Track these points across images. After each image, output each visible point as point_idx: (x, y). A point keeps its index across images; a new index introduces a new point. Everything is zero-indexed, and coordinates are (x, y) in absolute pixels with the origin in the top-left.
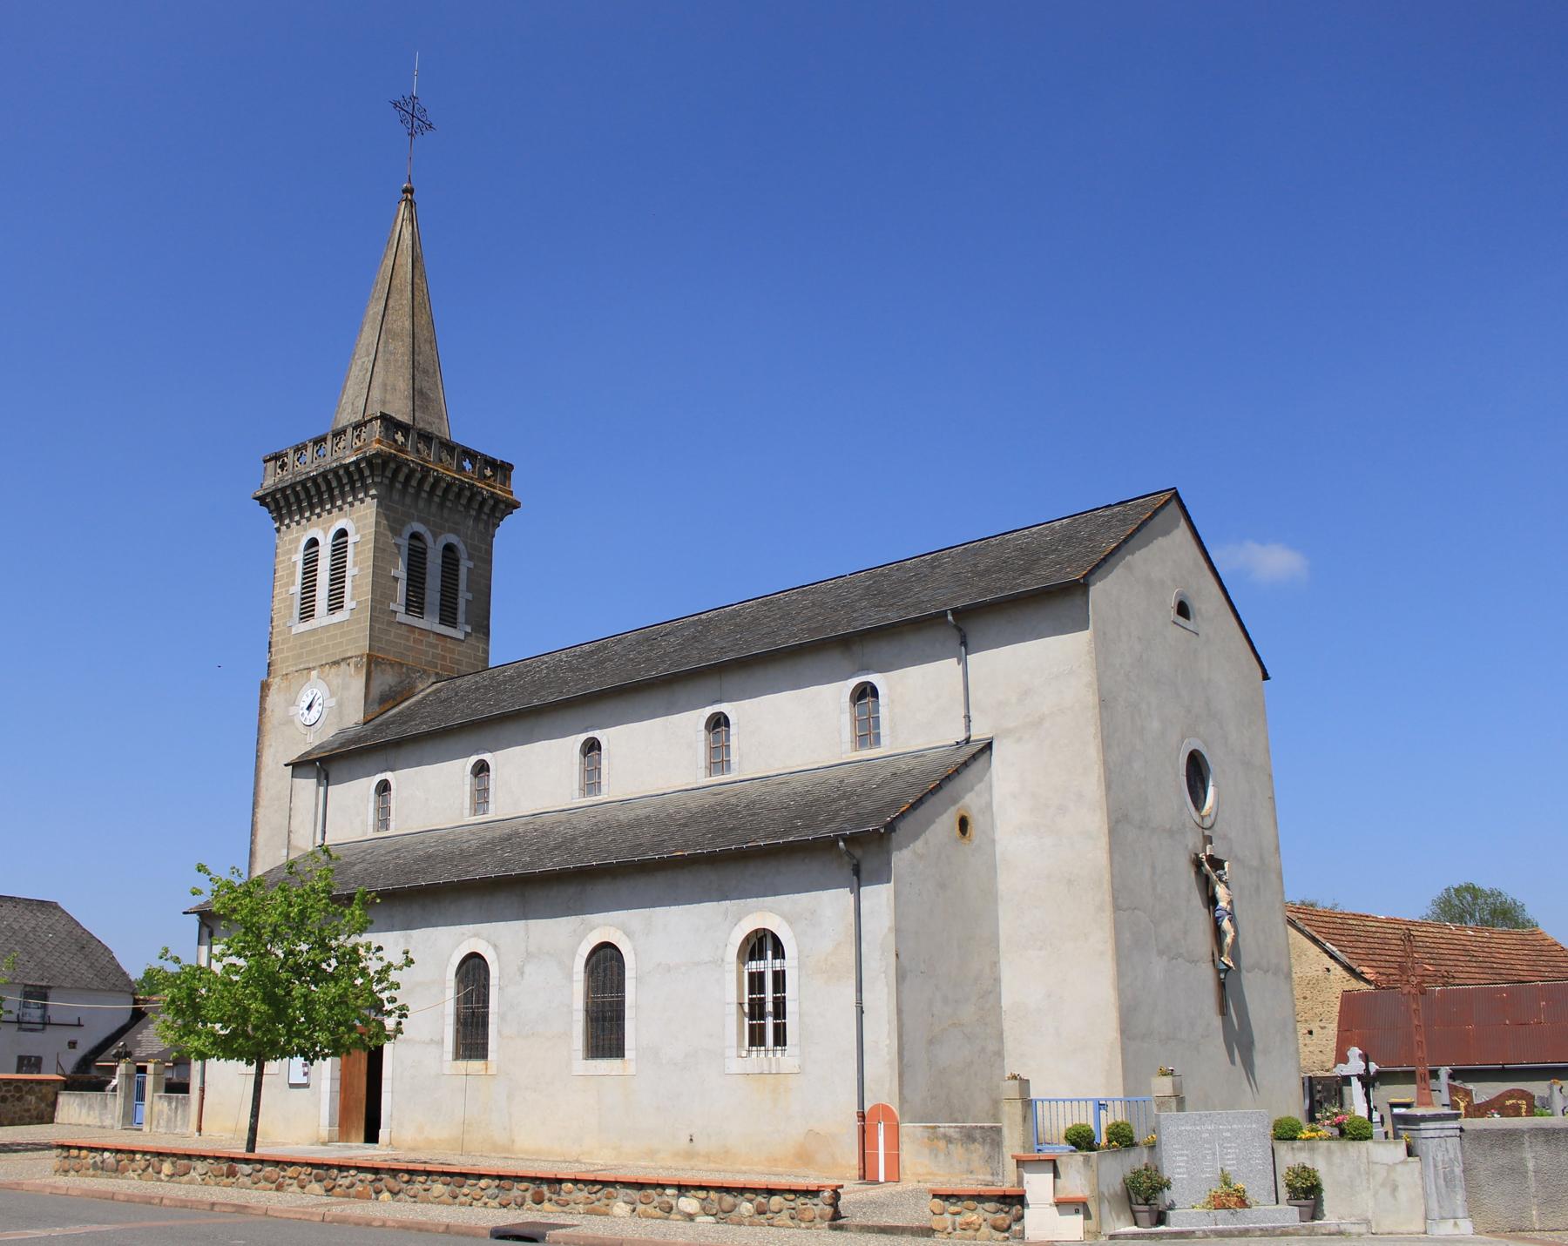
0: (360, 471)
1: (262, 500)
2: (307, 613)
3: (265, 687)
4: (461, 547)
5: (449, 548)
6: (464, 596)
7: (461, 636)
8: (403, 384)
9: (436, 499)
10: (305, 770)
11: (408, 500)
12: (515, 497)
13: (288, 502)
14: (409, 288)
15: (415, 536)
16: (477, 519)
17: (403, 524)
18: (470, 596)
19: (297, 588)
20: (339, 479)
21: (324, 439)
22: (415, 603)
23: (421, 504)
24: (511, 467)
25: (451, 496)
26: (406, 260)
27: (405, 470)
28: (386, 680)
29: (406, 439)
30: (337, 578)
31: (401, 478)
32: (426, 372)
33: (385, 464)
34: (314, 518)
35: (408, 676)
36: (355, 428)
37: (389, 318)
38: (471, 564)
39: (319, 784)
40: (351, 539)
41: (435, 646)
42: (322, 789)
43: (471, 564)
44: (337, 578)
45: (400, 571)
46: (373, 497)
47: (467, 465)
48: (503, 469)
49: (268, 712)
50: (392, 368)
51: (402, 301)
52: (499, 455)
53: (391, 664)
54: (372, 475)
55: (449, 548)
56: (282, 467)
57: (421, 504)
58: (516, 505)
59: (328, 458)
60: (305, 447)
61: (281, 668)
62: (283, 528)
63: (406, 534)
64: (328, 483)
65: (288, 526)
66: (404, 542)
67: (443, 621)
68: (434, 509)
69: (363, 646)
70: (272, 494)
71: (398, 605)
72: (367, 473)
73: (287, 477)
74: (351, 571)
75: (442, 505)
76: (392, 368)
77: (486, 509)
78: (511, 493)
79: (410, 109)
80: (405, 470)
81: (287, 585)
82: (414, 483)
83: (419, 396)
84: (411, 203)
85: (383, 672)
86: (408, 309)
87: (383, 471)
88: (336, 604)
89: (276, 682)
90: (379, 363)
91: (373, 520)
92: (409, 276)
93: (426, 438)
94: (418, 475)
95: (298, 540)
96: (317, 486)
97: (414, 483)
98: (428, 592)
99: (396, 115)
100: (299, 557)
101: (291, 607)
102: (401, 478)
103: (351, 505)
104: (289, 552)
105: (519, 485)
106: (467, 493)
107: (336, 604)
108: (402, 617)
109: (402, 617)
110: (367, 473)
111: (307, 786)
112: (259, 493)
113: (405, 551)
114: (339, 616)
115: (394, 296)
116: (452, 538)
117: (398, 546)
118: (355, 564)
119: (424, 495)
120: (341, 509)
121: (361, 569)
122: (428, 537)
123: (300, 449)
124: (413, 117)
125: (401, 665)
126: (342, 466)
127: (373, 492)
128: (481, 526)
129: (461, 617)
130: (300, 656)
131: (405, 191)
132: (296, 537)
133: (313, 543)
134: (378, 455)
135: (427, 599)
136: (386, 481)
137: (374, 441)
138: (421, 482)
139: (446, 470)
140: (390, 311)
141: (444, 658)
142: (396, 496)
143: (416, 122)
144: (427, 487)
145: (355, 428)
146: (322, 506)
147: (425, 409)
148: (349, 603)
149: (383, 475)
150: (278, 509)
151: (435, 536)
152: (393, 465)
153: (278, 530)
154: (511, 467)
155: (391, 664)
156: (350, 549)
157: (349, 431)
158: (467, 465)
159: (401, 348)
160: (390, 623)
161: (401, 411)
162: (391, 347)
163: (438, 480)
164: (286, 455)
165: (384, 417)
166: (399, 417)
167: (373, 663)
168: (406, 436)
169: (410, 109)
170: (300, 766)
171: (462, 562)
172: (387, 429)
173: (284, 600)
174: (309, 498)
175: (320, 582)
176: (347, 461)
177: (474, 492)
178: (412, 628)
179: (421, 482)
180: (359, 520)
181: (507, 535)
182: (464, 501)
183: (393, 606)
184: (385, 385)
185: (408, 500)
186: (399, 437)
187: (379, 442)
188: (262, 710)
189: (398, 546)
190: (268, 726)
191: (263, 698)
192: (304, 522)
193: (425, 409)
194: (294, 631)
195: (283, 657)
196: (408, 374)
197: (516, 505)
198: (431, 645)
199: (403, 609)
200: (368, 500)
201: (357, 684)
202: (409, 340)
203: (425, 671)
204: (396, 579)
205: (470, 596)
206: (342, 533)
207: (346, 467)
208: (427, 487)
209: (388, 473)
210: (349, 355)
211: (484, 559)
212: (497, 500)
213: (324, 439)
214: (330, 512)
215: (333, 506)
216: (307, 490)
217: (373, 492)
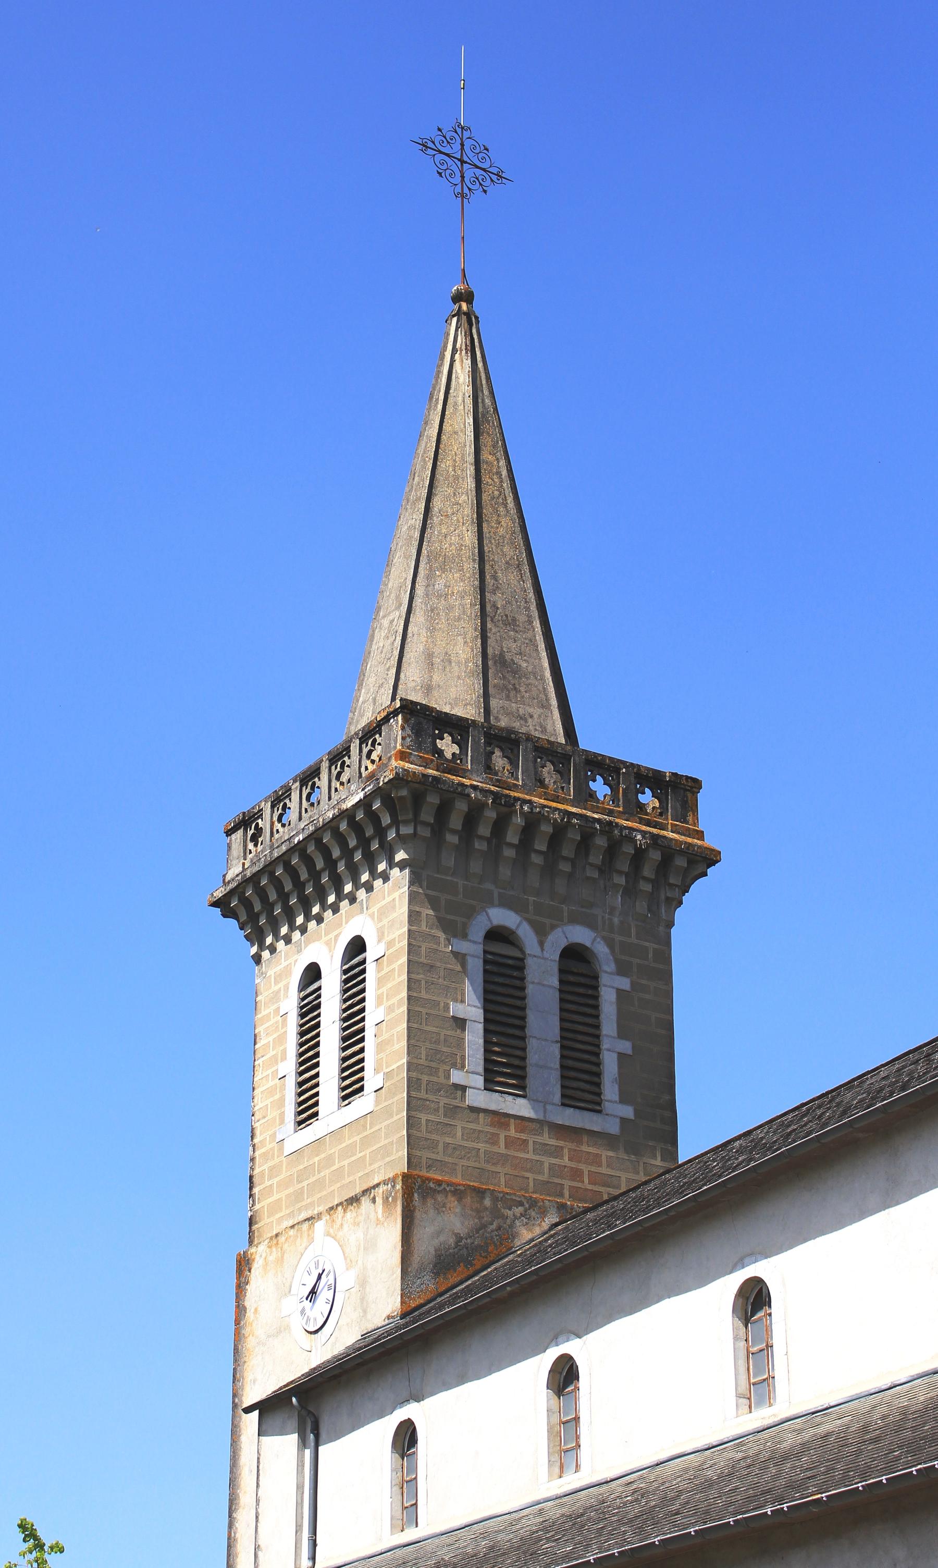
0: (373, 817)
1: (215, 904)
2: (307, 1111)
3: (243, 1264)
4: (601, 950)
5: (574, 956)
6: (612, 1049)
7: (613, 1128)
8: (463, 650)
9: (537, 859)
10: (276, 1419)
11: (476, 866)
12: (710, 841)
13: (267, 903)
14: (471, 470)
15: (496, 935)
16: (630, 892)
17: (470, 913)
18: (626, 1046)
19: (289, 1066)
20: (341, 839)
21: (314, 772)
22: (504, 1069)
23: (505, 872)
24: (696, 784)
25: (567, 851)
26: (462, 422)
27: (461, 806)
28: (447, 1224)
29: (462, 745)
30: (353, 1036)
31: (456, 821)
32: (510, 622)
33: (418, 799)
34: (312, 925)
35: (496, 1214)
36: (363, 740)
37: (433, 533)
38: (624, 983)
39: (303, 1443)
40: (371, 954)
41: (557, 1152)
42: (308, 1453)
43: (624, 983)
44: (353, 1036)
45: (470, 1007)
46: (402, 865)
47: (599, 787)
48: (680, 791)
49: (250, 1314)
50: (442, 624)
51: (456, 499)
52: (666, 763)
53: (459, 1193)
54: (396, 823)
55: (574, 956)
56: (254, 839)
57: (505, 872)
58: (711, 858)
59: (324, 805)
60: (287, 791)
61: (268, 1225)
62: (266, 954)
63: (478, 929)
64: (325, 851)
65: (273, 949)
66: (473, 948)
67: (569, 1099)
68: (534, 879)
69: (396, 1160)
70: (237, 891)
71: (469, 1074)
72: (386, 820)
73: (263, 852)
74: (373, 1014)
75: (549, 870)
76: (442, 624)
77: (648, 871)
78: (700, 835)
79: (455, 149)
80: (461, 806)
81: (275, 1060)
82: (484, 830)
83: (493, 667)
84: (470, 320)
85: (440, 1209)
86: (468, 511)
87: (416, 814)
88: (351, 1088)
89: (260, 1253)
90: (418, 617)
91: (405, 909)
92: (470, 449)
93: (508, 741)
94: (491, 814)
95: (287, 971)
96: (308, 861)
97: (484, 830)
98: (532, 1045)
99: (427, 164)
100: (291, 1003)
101: (281, 1102)
102: (456, 821)
103: (369, 888)
104: (275, 997)
105: (714, 822)
106: (601, 841)
107: (351, 1088)
108: (478, 1097)
109: (478, 1097)
110: (386, 820)
111: (284, 1447)
112: (219, 894)
113: (476, 965)
114: (362, 1105)
115: (442, 490)
116: (580, 935)
117: (460, 957)
118: (379, 1001)
119: (509, 853)
120: (353, 899)
121: (390, 1009)
122: (526, 934)
123: (279, 799)
124: (464, 163)
125: (480, 1193)
126: (343, 814)
127: (400, 856)
128: (641, 906)
129: (610, 1090)
130: (298, 1196)
131: (457, 298)
132: (287, 962)
133: (313, 973)
134: (399, 780)
135: (533, 1057)
136: (425, 832)
137: (392, 755)
138: (500, 826)
139: (552, 799)
140: (435, 519)
141: (576, 1174)
142: (449, 860)
143: (469, 173)
144: (512, 837)
145: (363, 740)
146: (321, 897)
147: (510, 691)
148: (372, 1080)
149: (416, 821)
150: (253, 918)
151: (542, 932)
152: (433, 799)
153: (257, 959)
154: (696, 784)
155: (459, 1193)
156: (370, 967)
157: (355, 747)
158: (599, 787)
159: (458, 584)
160: (452, 1111)
161: (457, 696)
162: (440, 584)
163: (533, 821)
164: (259, 814)
165: (409, 710)
166: (459, 711)
167: (416, 1191)
168: (461, 743)
169: (455, 149)
170: (270, 1409)
171: (604, 979)
172: (418, 732)
173: (271, 1091)
174: (299, 886)
175: (328, 1053)
176: (349, 804)
177: (616, 840)
178: (500, 1118)
179: (500, 826)
180: (380, 913)
181: (699, 925)
182: (596, 858)
183: (457, 1077)
184: (429, 656)
185: (476, 866)
186: (447, 746)
187: (402, 756)
188: (240, 1310)
189: (460, 957)
190: (250, 1343)
191: (240, 1289)
192: (296, 935)
193: (510, 691)
194: (289, 1148)
195: (275, 1204)
196: (470, 628)
197: (711, 858)
198: (544, 1149)
199: (479, 1081)
200: (395, 872)
201: (389, 1236)
202: (470, 567)
203: (533, 1203)
204: (460, 1023)
205: (626, 1046)
206: (357, 946)
207: (348, 815)
208: (512, 837)
209: (427, 816)
210: (373, 611)
211: (653, 973)
212: (668, 851)
213: (314, 772)
214: (335, 909)
215: (340, 897)
216: (292, 872)
217: (400, 856)
